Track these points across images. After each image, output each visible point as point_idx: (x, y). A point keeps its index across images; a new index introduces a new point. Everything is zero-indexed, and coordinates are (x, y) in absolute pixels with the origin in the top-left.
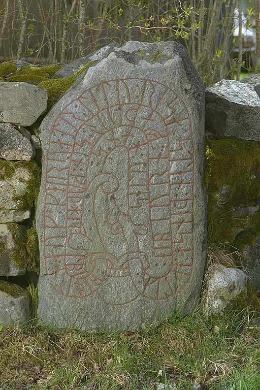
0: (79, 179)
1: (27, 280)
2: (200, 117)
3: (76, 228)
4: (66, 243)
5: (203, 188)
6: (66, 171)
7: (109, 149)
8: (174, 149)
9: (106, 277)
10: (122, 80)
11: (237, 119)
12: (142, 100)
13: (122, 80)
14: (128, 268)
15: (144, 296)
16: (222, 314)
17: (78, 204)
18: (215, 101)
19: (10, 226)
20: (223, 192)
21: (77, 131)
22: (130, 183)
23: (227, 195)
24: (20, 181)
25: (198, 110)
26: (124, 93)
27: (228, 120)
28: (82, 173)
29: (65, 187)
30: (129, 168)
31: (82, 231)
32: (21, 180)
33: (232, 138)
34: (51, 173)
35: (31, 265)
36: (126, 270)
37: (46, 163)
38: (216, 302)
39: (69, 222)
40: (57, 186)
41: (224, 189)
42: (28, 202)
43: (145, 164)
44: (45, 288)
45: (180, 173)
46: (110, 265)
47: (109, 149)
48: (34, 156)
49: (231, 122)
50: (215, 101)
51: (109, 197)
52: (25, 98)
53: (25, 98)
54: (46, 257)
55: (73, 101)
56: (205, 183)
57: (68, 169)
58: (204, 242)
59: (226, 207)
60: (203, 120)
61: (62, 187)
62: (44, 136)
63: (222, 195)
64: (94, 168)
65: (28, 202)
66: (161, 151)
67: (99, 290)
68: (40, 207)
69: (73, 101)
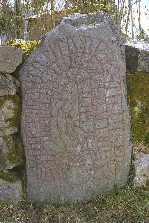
0: (46, 105)
1: (20, 172)
2: (123, 59)
3: (46, 137)
4: (40, 147)
5: (128, 105)
6: (37, 101)
7: (65, 84)
8: (108, 81)
9: (69, 167)
10: (70, 38)
11: (144, 60)
12: (109, 104)
13: (70, 38)
14: (83, 161)
15: (94, 178)
16: (145, 186)
17: (47, 122)
18: (130, 50)
19: (5, 138)
20: (140, 106)
21: (42, 73)
22: (80, 106)
23: (142, 108)
24: (8, 109)
25: (122, 54)
26: (72, 46)
27: (139, 61)
28: (48, 101)
29: (38, 111)
30: (78, 96)
31: (51, 139)
32: (9, 108)
33: (142, 72)
34: (28, 103)
35: (21, 162)
36: (81, 163)
37: (26, 97)
38: (141, 178)
39: (43, 134)
40: (32, 111)
41: (140, 104)
42: (17, 122)
43: (88, 93)
44: (31, 176)
45: (113, 96)
46: (71, 160)
47: (65, 84)
48: (17, 91)
49: (141, 62)
50: (130, 50)
51: (67, 116)
52: (7, 55)
53: (7, 55)
54: (29, 157)
55: (38, 54)
56: (129, 103)
57: (38, 99)
58: (130, 140)
59: (141, 115)
60: (125, 60)
61: (35, 111)
62: (24, 77)
63: (139, 108)
64: (55, 98)
65: (17, 122)
66: (99, 83)
67: (64, 176)
68: (23, 124)
69: (38, 54)
